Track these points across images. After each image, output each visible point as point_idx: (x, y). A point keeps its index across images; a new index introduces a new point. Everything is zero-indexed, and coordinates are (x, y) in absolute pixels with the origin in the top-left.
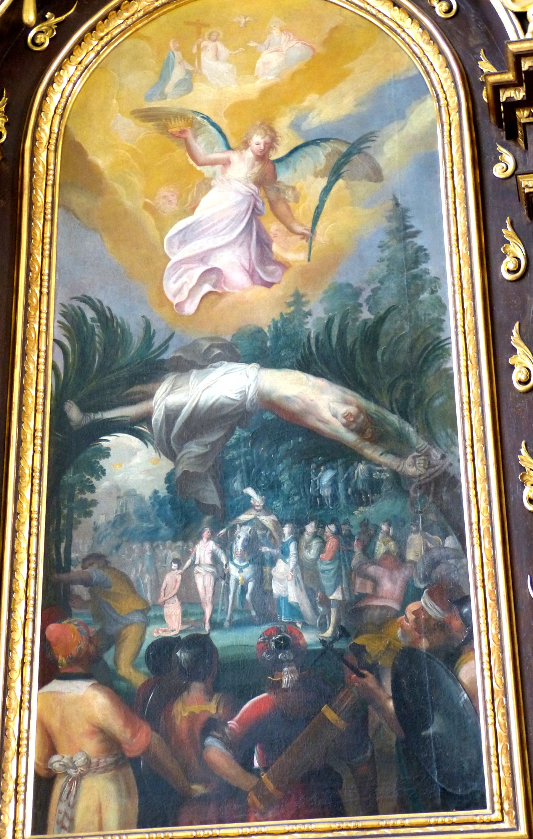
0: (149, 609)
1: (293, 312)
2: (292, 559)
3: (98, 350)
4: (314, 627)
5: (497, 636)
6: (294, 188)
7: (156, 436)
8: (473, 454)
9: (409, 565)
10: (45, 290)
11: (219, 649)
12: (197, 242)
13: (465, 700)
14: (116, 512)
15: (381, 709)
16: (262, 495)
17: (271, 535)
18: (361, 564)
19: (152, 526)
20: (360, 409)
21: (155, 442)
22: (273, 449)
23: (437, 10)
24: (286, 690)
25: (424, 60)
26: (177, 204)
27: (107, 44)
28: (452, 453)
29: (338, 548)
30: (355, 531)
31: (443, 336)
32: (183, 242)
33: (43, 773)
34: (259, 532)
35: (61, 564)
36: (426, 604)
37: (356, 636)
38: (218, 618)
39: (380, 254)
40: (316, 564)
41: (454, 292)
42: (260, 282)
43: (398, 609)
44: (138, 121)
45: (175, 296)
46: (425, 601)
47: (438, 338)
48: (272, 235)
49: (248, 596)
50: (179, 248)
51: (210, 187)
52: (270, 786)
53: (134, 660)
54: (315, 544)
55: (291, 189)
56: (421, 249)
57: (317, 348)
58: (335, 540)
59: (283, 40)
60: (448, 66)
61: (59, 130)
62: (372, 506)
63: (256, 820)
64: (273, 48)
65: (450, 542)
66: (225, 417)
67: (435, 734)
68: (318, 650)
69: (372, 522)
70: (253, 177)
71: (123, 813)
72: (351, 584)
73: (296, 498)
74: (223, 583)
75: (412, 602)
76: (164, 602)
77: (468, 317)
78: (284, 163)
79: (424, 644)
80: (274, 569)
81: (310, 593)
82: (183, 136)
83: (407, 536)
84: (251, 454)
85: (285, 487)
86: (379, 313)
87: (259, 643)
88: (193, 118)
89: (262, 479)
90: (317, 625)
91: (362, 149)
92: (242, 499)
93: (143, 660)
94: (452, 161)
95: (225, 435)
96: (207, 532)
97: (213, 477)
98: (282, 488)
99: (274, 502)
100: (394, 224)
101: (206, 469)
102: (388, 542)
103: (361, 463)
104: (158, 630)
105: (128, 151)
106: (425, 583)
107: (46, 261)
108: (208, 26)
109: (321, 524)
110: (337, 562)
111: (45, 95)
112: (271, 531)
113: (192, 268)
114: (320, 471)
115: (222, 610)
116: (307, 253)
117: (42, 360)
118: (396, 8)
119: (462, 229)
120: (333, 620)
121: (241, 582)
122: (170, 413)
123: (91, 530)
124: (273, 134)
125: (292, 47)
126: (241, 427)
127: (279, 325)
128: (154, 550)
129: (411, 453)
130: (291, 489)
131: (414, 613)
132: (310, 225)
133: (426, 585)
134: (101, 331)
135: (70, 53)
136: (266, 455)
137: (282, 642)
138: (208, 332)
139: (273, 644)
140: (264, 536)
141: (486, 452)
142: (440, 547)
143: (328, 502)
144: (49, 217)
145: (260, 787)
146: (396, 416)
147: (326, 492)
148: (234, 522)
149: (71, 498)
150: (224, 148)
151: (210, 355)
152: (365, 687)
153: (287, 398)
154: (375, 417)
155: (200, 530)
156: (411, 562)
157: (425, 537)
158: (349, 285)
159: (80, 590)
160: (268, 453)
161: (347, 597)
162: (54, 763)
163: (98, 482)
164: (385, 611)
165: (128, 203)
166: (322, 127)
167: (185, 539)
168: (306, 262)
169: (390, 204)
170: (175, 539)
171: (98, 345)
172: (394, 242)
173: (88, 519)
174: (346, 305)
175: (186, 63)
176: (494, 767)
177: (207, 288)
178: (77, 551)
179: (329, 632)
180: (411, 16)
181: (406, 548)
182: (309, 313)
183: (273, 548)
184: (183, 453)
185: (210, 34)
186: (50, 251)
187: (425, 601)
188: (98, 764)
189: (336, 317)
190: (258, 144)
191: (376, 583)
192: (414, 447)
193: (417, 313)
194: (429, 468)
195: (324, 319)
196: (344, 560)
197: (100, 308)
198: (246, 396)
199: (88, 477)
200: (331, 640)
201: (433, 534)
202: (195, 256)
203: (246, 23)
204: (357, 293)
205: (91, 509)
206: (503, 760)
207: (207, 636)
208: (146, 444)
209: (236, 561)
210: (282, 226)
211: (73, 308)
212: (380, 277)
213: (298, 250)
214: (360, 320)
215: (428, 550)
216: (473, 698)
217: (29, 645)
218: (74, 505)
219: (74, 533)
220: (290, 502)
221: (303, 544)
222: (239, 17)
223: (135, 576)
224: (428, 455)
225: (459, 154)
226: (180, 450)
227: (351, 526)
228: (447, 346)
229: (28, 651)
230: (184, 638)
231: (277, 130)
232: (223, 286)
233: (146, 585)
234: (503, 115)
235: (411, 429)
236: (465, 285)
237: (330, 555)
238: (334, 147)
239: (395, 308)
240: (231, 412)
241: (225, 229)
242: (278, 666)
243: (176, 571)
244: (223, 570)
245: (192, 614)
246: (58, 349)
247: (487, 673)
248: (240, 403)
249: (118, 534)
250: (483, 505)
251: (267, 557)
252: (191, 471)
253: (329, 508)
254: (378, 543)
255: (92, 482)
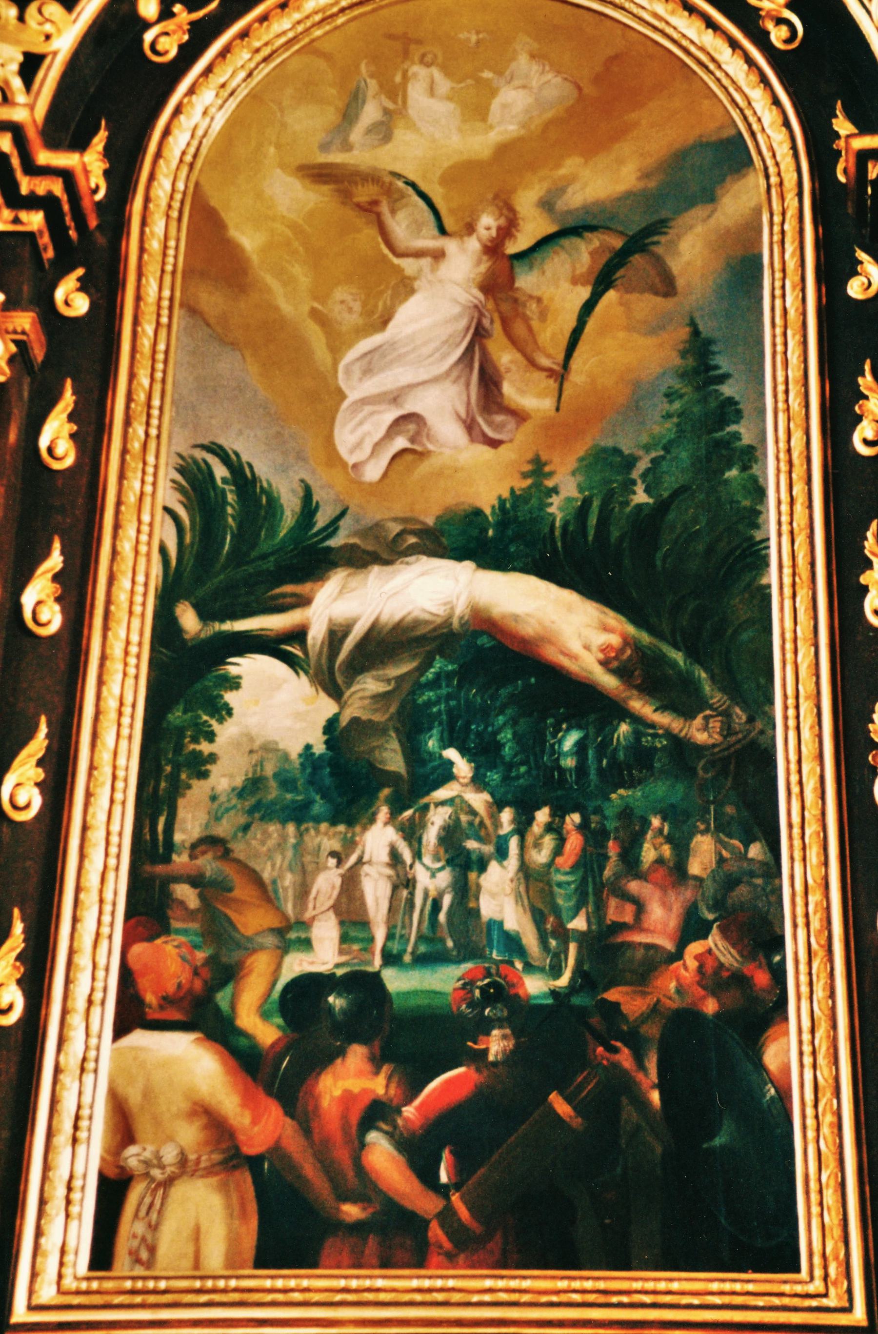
0: (289, 928)
1: (530, 487)
2: (512, 862)
3: (231, 528)
4: (542, 970)
5: (827, 1002)
6: (539, 300)
7: (313, 662)
8: (798, 717)
9: (691, 882)
10: (153, 432)
11: (394, 996)
12: (389, 373)
13: (772, 1098)
14: (246, 775)
15: (643, 1104)
16: (469, 761)
17: (482, 823)
18: (617, 876)
19: (300, 798)
20: (627, 641)
21: (311, 671)
22: (490, 692)
23: (773, 38)
24: (495, 1064)
25: (748, 113)
26: (361, 314)
27: (266, 60)
28: (765, 713)
29: (584, 850)
30: (611, 825)
31: (758, 536)
32: (368, 371)
33: (112, 1173)
34: (464, 818)
35: (158, 849)
36: (716, 945)
37: (606, 989)
38: (395, 947)
39: (667, 406)
40: (549, 873)
41: (778, 470)
42: (481, 438)
43: (673, 951)
44: (307, 182)
45: (352, 451)
46: (714, 940)
47: (752, 538)
48: (502, 369)
49: (442, 917)
50: (360, 379)
51: (412, 291)
52: (463, 1213)
53: (261, 1006)
54: (549, 842)
55: (535, 300)
56: (731, 401)
57: (563, 543)
58: (580, 837)
59: (532, 73)
60: (786, 124)
61: (186, 187)
62: (639, 788)
63: (439, 1267)
64: (516, 83)
65: (756, 851)
66: (421, 640)
67: (722, 1147)
68: (547, 1005)
69: (638, 812)
70: (479, 279)
71: (233, 1241)
72: (600, 908)
73: (523, 769)
74: (405, 893)
75: (695, 941)
76: (313, 918)
77: (799, 508)
78: (526, 261)
79: (711, 1007)
80: (483, 876)
81: (538, 918)
82: (375, 209)
83: (691, 836)
84: (457, 698)
85: (507, 751)
86: (661, 495)
87: (455, 990)
88: (391, 184)
89: (472, 737)
90: (547, 968)
91: (647, 245)
92: (440, 765)
93: (276, 1006)
94: (784, 270)
95: (417, 669)
96: (384, 813)
97: (397, 730)
98: (503, 753)
99: (489, 774)
100: (691, 362)
101: (387, 716)
102: (662, 844)
103: (625, 722)
104: (301, 960)
105: (288, 227)
106: (715, 912)
107: (157, 387)
108: (419, 42)
109: (559, 812)
110: (580, 873)
111: (167, 132)
112: (481, 817)
113: (379, 412)
114: (560, 730)
115: (402, 936)
116: (555, 399)
117: (144, 538)
118: (710, 31)
119: (795, 373)
120: (571, 961)
121: (433, 893)
122: (336, 628)
123: (207, 799)
124: (511, 216)
125: (546, 83)
126: (442, 656)
127: (508, 505)
128: (301, 835)
129: (702, 710)
130: (515, 755)
131: (697, 957)
132: (561, 357)
133: (717, 915)
134: (235, 498)
135: (208, 70)
136: (479, 700)
137: (492, 991)
138: (399, 509)
139: (477, 993)
140: (471, 824)
141: (819, 714)
142: (741, 858)
143: (571, 778)
144: (164, 320)
145: (447, 1216)
146: (680, 654)
147: (569, 762)
148: (425, 800)
149: (179, 748)
150: (435, 232)
151: (402, 545)
152: (616, 1066)
153: (516, 618)
154: (649, 652)
155: (374, 809)
156: (696, 878)
157: (719, 841)
158: (617, 451)
159: (185, 893)
160: (482, 698)
161: (594, 927)
162: (130, 1156)
163: (221, 726)
164: (652, 952)
165: (286, 307)
166: (586, 209)
167: (351, 822)
168: (553, 413)
169: (684, 333)
170: (334, 822)
171: (230, 520)
172: (687, 390)
173: (202, 783)
174: (612, 482)
175: (383, 97)
176: (815, 1210)
177: (401, 443)
178: (184, 831)
179: (564, 981)
180: (734, 44)
181: (688, 856)
182: (555, 490)
183: (485, 844)
184: (353, 689)
185: (423, 56)
186: (164, 372)
187: (714, 940)
188: (198, 1161)
189: (594, 499)
190: (488, 229)
191: (640, 907)
192: (707, 702)
193: (718, 499)
194: (729, 734)
195: (576, 500)
196: (592, 870)
197: (236, 464)
198: (452, 609)
199: (205, 718)
200: (567, 991)
201: (731, 838)
202: (385, 393)
203: (478, 42)
204: (630, 462)
205: (209, 767)
206: (830, 1198)
207: (377, 976)
208: (297, 673)
209: (427, 859)
210: (518, 356)
211: (195, 462)
212: (664, 441)
213: (540, 395)
214: (633, 504)
215: (721, 860)
216: (784, 1096)
217: (100, 974)
218: (181, 759)
219: (181, 802)
220: (513, 774)
221: (530, 840)
222: (469, 32)
223: (270, 874)
224: (727, 714)
225: (795, 259)
226: (349, 685)
227: (605, 818)
228: (764, 552)
229: (99, 985)
230: (341, 976)
231: (518, 208)
232: (425, 440)
233: (285, 889)
234: (869, 202)
235: (704, 675)
236: (796, 460)
237: (572, 860)
238: (605, 240)
239: (686, 490)
240: (429, 632)
241: (430, 356)
242: (484, 1027)
243: (335, 870)
244: (406, 874)
245: (355, 940)
246: (169, 522)
247: (808, 1060)
248: (444, 619)
249: (247, 808)
250: (810, 796)
251: (474, 857)
252: (364, 717)
253: (571, 787)
254: (646, 846)
255: (210, 726)
